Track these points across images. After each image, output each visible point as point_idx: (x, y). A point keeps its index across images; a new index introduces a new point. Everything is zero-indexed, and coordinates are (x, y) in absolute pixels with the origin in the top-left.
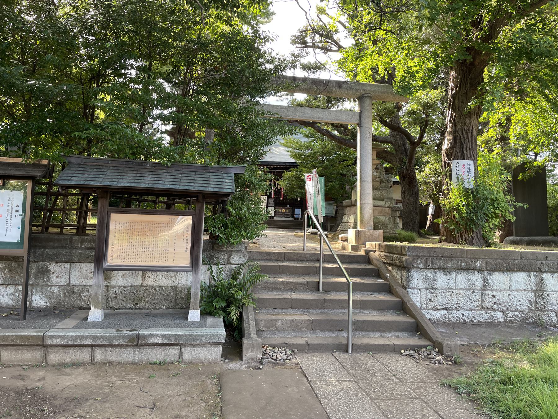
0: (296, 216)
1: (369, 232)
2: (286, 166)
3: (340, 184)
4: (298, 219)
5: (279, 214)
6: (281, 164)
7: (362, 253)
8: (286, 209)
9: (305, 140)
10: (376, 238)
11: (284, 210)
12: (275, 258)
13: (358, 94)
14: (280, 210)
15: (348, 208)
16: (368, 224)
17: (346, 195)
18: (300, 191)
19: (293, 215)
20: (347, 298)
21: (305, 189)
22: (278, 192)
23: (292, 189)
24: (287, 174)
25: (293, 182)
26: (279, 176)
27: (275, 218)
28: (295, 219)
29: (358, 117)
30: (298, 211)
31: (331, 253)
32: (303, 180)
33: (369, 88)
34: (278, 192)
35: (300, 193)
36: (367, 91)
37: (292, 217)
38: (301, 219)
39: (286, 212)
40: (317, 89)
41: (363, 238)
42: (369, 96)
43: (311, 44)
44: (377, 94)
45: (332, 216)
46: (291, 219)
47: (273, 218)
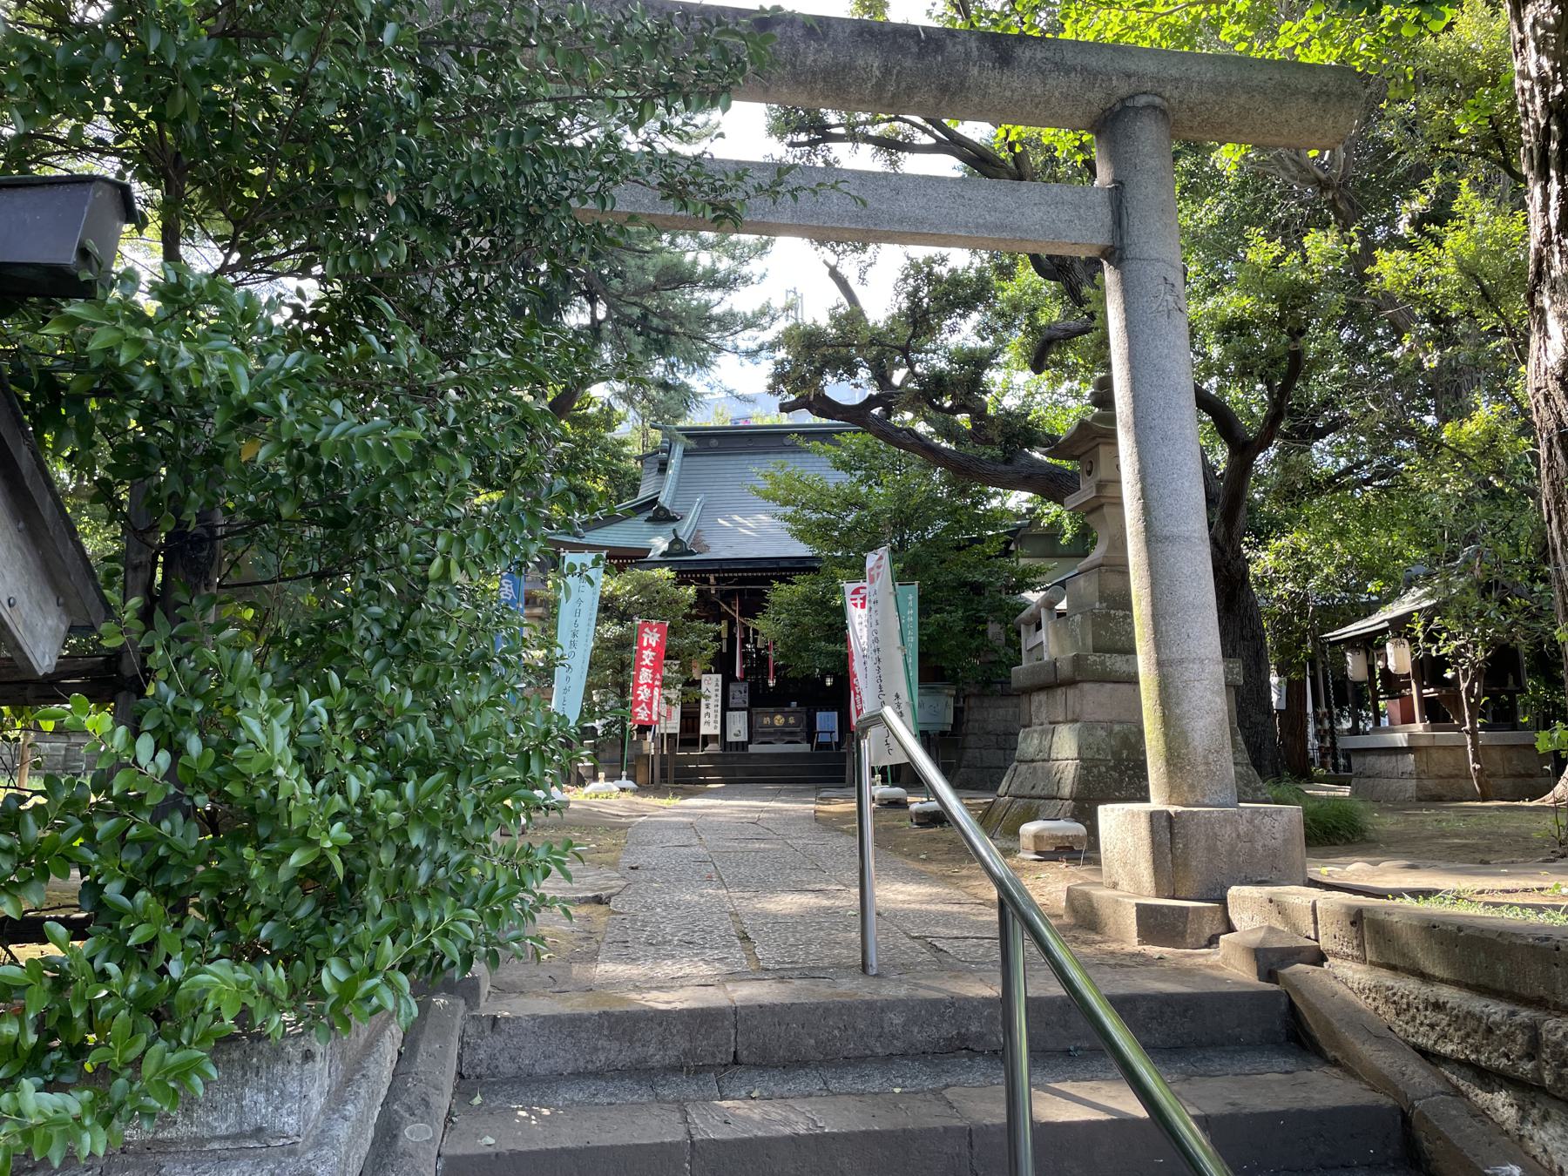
0: (823, 738)
1: (1227, 820)
2: (784, 569)
3: (967, 619)
4: (828, 746)
5: (764, 734)
6: (765, 565)
7: (1228, 965)
8: (786, 715)
9: (837, 480)
10: (1274, 853)
11: (779, 720)
12: (671, 1056)
13: (1097, 98)
14: (767, 720)
15: (1039, 698)
16: (1210, 775)
17: (992, 658)
18: (831, 647)
19: (811, 734)
20: (994, 991)
21: (845, 640)
22: (757, 665)
23: (799, 644)
24: (780, 593)
25: (806, 620)
26: (754, 605)
27: (753, 748)
28: (821, 746)
29: (1105, 214)
30: (827, 721)
31: (1057, 990)
32: (841, 612)
33: (1151, 67)
34: (757, 665)
35: (831, 654)
36: (1141, 77)
37: (810, 740)
38: (839, 745)
39: (786, 724)
40: (887, 71)
41: (1198, 860)
42: (1155, 107)
43: (841, 131)
44: (1194, 96)
45: (943, 733)
46: (804, 747)
47: (742, 746)
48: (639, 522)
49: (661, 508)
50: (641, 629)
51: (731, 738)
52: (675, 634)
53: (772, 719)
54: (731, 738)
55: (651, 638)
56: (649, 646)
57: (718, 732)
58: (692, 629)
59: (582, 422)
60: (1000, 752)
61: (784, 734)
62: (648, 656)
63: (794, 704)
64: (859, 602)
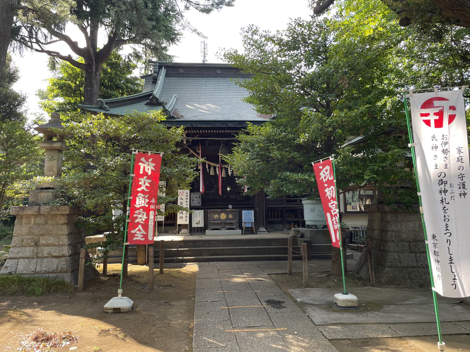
5: (214, 224)
6: (218, 125)
11: (223, 216)
14: (216, 216)
39: (227, 219)
48: (142, 105)
49: (154, 97)
50: (137, 160)
51: (194, 225)
52: (165, 165)
53: (219, 215)
54: (194, 225)
55: (147, 167)
56: (145, 174)
57: (187, 223)
58: (179, 161)
59: (114, 66)
60: (413, 255)
61: (228, 225)
62: (144, 183)
63: (230, 206)
64: (432, 118)
